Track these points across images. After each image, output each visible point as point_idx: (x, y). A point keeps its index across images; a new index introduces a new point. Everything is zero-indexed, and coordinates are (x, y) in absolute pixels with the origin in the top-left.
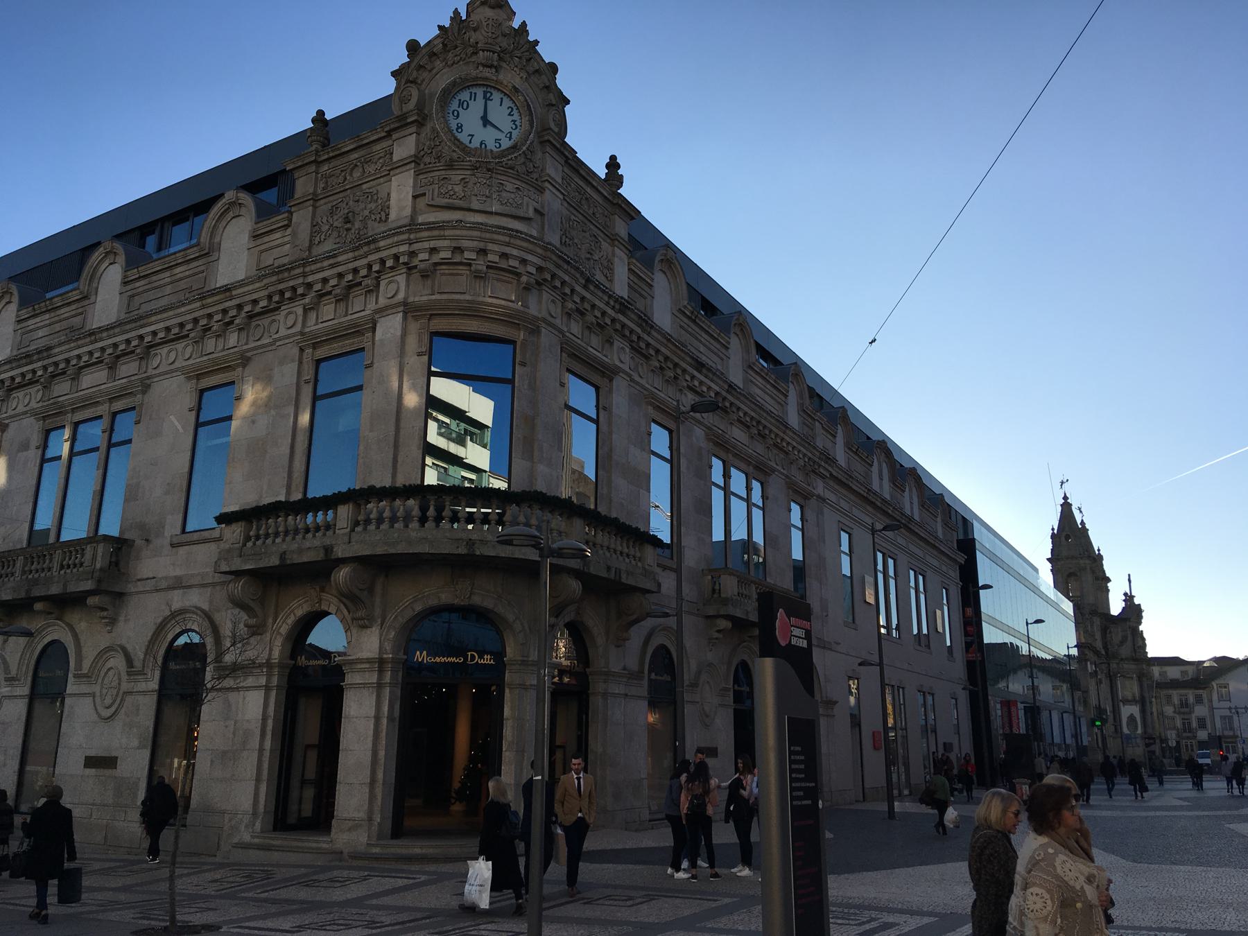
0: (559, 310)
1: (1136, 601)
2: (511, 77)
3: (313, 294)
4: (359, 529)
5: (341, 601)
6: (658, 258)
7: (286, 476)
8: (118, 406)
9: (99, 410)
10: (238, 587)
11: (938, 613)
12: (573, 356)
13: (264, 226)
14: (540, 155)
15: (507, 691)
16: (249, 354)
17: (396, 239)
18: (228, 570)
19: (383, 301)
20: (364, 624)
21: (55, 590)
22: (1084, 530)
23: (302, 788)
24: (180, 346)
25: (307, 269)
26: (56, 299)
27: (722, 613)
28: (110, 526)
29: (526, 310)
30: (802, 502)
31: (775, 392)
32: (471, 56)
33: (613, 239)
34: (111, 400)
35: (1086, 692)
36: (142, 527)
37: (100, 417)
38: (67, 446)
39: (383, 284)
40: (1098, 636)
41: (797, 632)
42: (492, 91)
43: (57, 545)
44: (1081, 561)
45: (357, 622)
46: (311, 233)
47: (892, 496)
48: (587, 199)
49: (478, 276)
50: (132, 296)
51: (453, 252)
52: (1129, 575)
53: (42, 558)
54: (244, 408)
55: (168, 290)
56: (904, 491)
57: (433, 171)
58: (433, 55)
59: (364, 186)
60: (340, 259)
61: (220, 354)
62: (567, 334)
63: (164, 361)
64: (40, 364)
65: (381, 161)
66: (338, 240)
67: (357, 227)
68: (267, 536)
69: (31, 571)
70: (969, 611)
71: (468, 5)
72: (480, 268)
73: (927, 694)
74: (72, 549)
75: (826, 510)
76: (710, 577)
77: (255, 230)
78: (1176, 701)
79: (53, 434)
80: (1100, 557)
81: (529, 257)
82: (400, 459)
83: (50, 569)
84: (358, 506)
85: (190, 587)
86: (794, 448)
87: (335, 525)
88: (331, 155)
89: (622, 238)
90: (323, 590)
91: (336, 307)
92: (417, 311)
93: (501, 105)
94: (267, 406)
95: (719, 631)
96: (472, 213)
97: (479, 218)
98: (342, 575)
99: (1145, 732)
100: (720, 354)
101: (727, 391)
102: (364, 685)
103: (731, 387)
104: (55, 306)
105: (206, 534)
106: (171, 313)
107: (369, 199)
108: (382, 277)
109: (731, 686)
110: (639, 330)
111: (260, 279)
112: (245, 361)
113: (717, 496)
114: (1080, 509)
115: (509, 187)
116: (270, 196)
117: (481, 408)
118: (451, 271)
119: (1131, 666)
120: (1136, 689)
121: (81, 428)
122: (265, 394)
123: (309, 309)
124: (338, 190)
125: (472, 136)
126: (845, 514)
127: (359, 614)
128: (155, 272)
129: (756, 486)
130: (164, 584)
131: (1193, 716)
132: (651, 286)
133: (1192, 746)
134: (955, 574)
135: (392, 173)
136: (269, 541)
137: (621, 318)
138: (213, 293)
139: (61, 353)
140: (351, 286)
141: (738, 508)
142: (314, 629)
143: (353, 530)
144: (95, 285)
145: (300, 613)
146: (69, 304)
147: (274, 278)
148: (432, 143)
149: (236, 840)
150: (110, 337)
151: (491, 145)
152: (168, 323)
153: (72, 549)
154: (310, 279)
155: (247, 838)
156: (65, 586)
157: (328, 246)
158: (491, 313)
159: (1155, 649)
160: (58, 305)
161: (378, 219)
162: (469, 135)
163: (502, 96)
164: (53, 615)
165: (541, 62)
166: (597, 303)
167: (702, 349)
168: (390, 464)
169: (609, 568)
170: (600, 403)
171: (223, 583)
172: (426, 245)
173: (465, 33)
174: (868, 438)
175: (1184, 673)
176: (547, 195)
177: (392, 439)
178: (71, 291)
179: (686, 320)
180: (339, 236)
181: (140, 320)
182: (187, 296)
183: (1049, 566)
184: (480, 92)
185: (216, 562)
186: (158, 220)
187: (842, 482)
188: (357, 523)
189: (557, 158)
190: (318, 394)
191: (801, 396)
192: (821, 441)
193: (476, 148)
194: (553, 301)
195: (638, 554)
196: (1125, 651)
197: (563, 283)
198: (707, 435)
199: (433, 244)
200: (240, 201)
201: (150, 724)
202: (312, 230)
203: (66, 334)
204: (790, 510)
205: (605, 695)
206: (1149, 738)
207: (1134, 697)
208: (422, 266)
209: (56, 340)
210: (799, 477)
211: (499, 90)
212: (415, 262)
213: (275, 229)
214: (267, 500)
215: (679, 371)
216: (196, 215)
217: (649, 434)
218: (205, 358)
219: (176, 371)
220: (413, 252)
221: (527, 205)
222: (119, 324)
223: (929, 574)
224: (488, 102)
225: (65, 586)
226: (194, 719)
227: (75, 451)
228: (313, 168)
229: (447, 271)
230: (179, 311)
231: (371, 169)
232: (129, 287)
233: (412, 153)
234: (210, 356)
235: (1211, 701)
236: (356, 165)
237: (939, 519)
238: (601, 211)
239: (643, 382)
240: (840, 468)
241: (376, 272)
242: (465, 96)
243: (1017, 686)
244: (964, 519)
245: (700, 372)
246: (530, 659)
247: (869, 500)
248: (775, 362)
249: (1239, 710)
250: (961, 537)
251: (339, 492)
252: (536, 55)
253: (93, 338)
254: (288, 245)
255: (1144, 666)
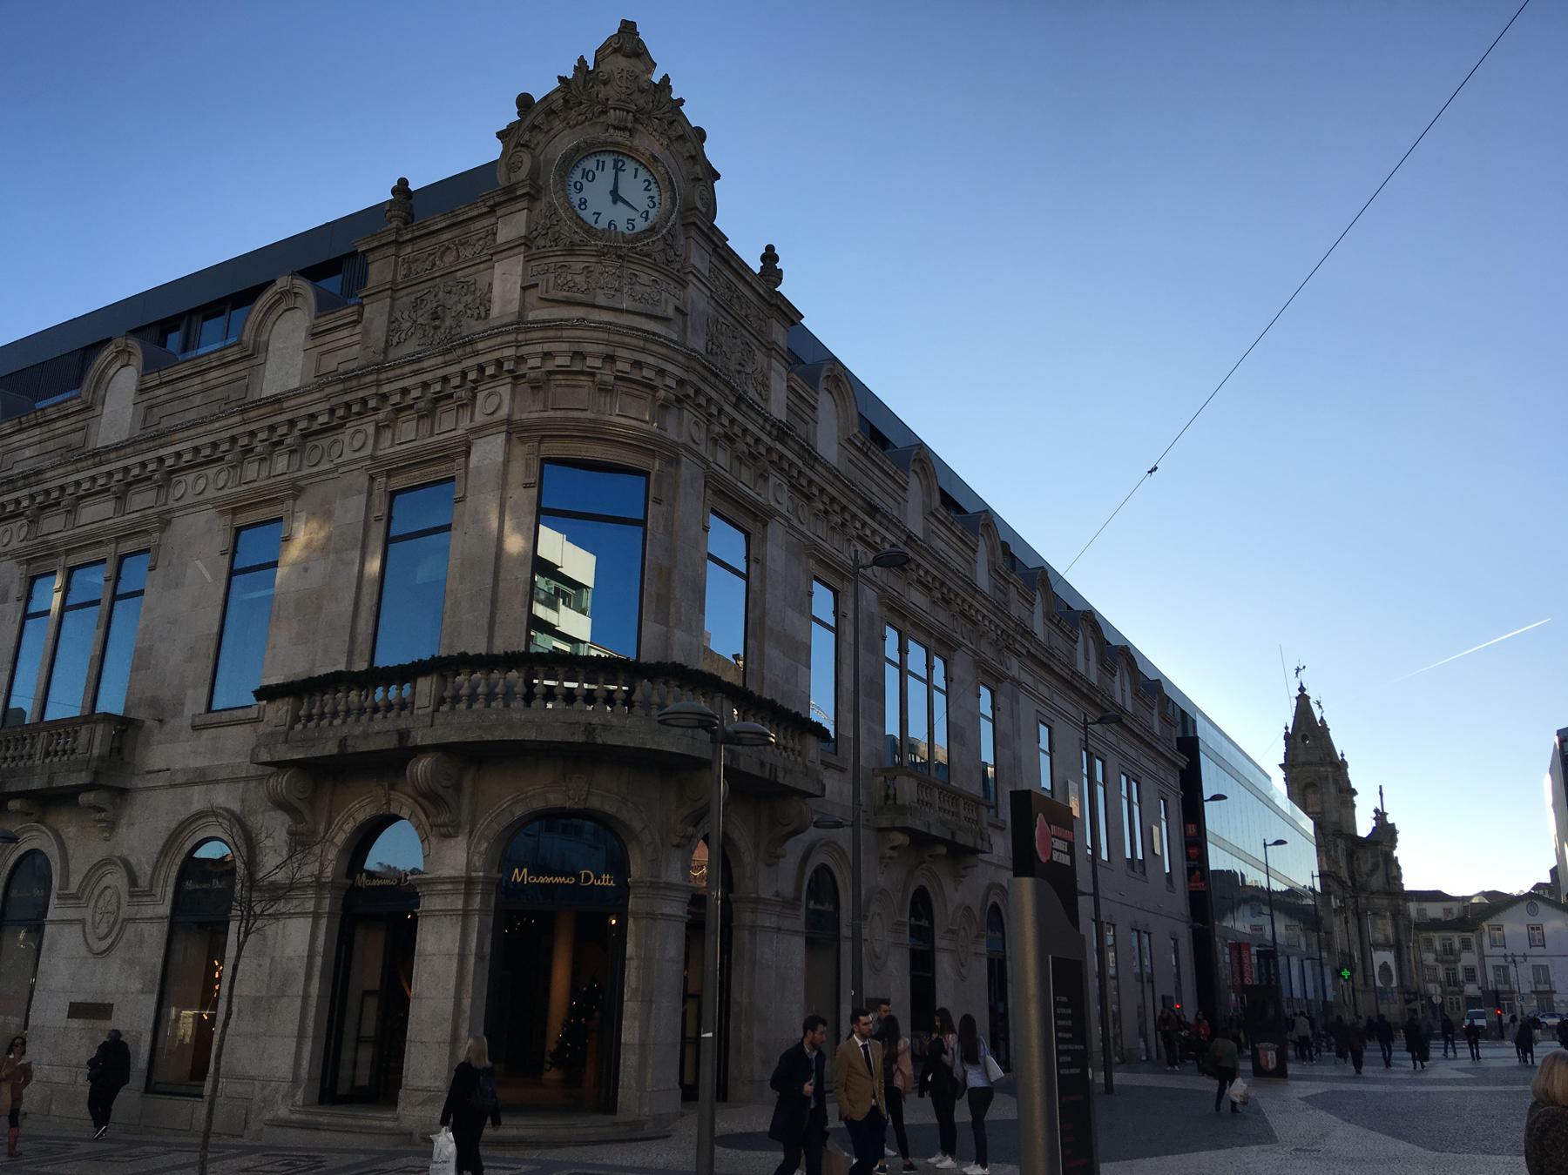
0: (703, 436)
1: (1390, 820)
2: (647, 142)
3: (390, 408)
4: (444, 708)
5: (416, 801)
6: (824, 374)
7: (348, 639)
8: (128, 546)
9: (101, 553)
10: (281, 782)
11: (1156, 830)
12: (719, 493)
13: (326, 322)
14: (682, 241)
15: (631, 921)
16: (302, 483)
17: (499, 340)
18: (269, 759)
19: (480, 419)
20: (447, 833)
21: (36, 784)
22: (1324, 730)
23: (356, 1049)
24: (211, 471)
25: (383, 376)
26: (49, 410)
27: (898, 824)
28: (112, 701)
29: (663, 433)
30: (994, 686)
31: (962, 546)
32: (598, 117)
33: (770, 348)
34: (118, 540)
35: (1329, 933)
36: (154, 703)
37: (103, 561)
38: (57, 597)
39: (480, 396)
40: (1343, 864)
41: (1059, 844)
42: (625, 159)
43: (42, 726)
44: (1322, 769)
45: (438, 829)
46: (388, 332)
47: (1099, 681)
48: (738, 297)
49: (604, 389)
50: (151, 407)
51: (572, 358)
52: (1381, 787)
53: (21, 742)
54: (294, 552)
55: (198, 400)
56: (1114, 675)
57: (549, 256)
58: (551, 112)
59: (459, 274)
60: (425, 364)
61: (266, 482)
62: (712, 465)
63: (190, 490)
64: (26, 492)
65: (481, 243)
66: (422, 341)
67: (447, 323)
68: (322, 716)
69: (22, 757)
70: (1192, 829)
71: (597, 52)
72: (606, 378)
73: (1142, 934)
74: (62, 730)
75: (1021, 697)
76: (883, 779)
77: (314, 326)
78: (1438, 945)
79: (39, 582)
80: (1344, 764)
81: (669, 367)
82: (499, 618)
83: (30, 756)
84: (444, 678)
85: (216, 782)
86: (984, 617)
87: (413, 703)
88: (417, 234)
89: (780, 347)
90: (392, 787)
91: (418, 424)
92: (526, 431)
93: (635, 177)
94: (323, 549)
95: (893, 848)
96: (597, 310)
97: (606, 317)
98: (421, 767)
99: (1401, 984)
100: (897, 496)
101: (906, 543)
102: (446, 913)
103: (910, 538)
104: (47, 418)
105: (240, 713)
106: (201, 430)
107: (465, 290)
108: (480, 389)
109: (907, 920)
110: (800, 464)
111: (320, 387)
112: (297, 491)
113: (891, 675)
114: (1319, 703)
115: (644, 279)
116: (333, 284)
117: (579, 564)
118: (568, 382)
119: (1384, 902)
120: (1390, 931)
121: (77, 574)
122: (322, 534)
123: (383, 426)
124: (425, 279)
125: (599, 214)
126: (1042, 701)
127: (441, 820)
128: (181, 377)
129: (938, 663)
130: (180, 779)
131: (1459, 965)
132: (814, 408)
133: (1458, 1003)
134: (1174, 781)
135: (494, 258)
136: (325, 723)
137: (779, 446)
138: (259, 404)
139: (492, 350)
140: (438, 399)
141: (917, 690)
142: (378, 840)
143: (436, 710)
144: (102, 393)
145: (361, 817)
146: (66, 416)
147: (340, 387)
148: (548, 222)
149: (269, 1116)
150: (119, 459)
151: (622, 226)
152: (197, 442)
153: (62, 730)
154: (386, 389)
155: (283, 1112)
156: (51, 779)
157: (410, 347)
158: (619, 436)
159: (1412, 880)
160: (54, 416)
161: (476, 315)
162: (595, 213)
163: (637, 166)
164: (33, 817)
165: (686, 126)
166: (750, 427)
167: (875, 489)
168: (486, 626)
169: (762, 764)
170: (752, 552)
171: (260, 778)
172: (538, 348)
173: (592, 87)
174: (1069, 608)
175: (1448, 911)
176: (691, 289)
177: (489, 594)
178: (70, 399)
179: (855, 452)
180: (424, 336)
181: (161, 437)
182: (222, 408)
183: (1282, 774)
184: (609, 161)
185: (253, 750)
186: (184, 312)
187: (1042, 662)
188: (442, 701)
189: (703, 244)
190: (391, 535)
191: (992, 552)
192: (1016, 609)
193: (604, 230)
194: (696, 423)
195: (798, 747)
196: (1377, 882)
197: (710, 400)
198: (879, 598)
199: (547, 347)
200: (296, 290)
201: (158, 960)
202: (388, 327)
203: (62, 455)
204: (979, 696)
205: (753, 928)
206: (1409, 993)
207: (1387, 938)
208: (532, 374)
209: (48, 462)
210: (989, 653)
211: (633, 158)
212: (523, 369)
213: (339, 326)
214: (321, 671)
215: (847, 516)
216: (235, 307)
217: (810, 595)
218: (245, 487)
219: (205, 504)
220: (522, 357)
221: (666, 301)
222: (132, 442)
223: (1144, 780)
224: (619, 173)
225: (51, 779)
226: (216, 950)
227: (118, 593)
228: (392, 250)
229: (563, 382)
230: (209, 427)
231: (468, 252)
232: (146, 396)
233: (523, 233)
234: (251, 485)
235: (1481, 946)
236: (448, 248)
237: (1155, 712)
238: (755, 313)
239: (803, 528)
240: (1038, 643)
241: (473, 381)
242: (590, 164)
243: (1240, 923)
244: (1183, 711)
245: (873, 518)
246: (663, 880)
247: (1072, 684)
248: (959, 509)
249: (1516, 959)
250: (1180, 735)
251: (420, 660)
252: (680, 118)
253: (97, 460)
254: (357, 347)
255: (1400, 902)
